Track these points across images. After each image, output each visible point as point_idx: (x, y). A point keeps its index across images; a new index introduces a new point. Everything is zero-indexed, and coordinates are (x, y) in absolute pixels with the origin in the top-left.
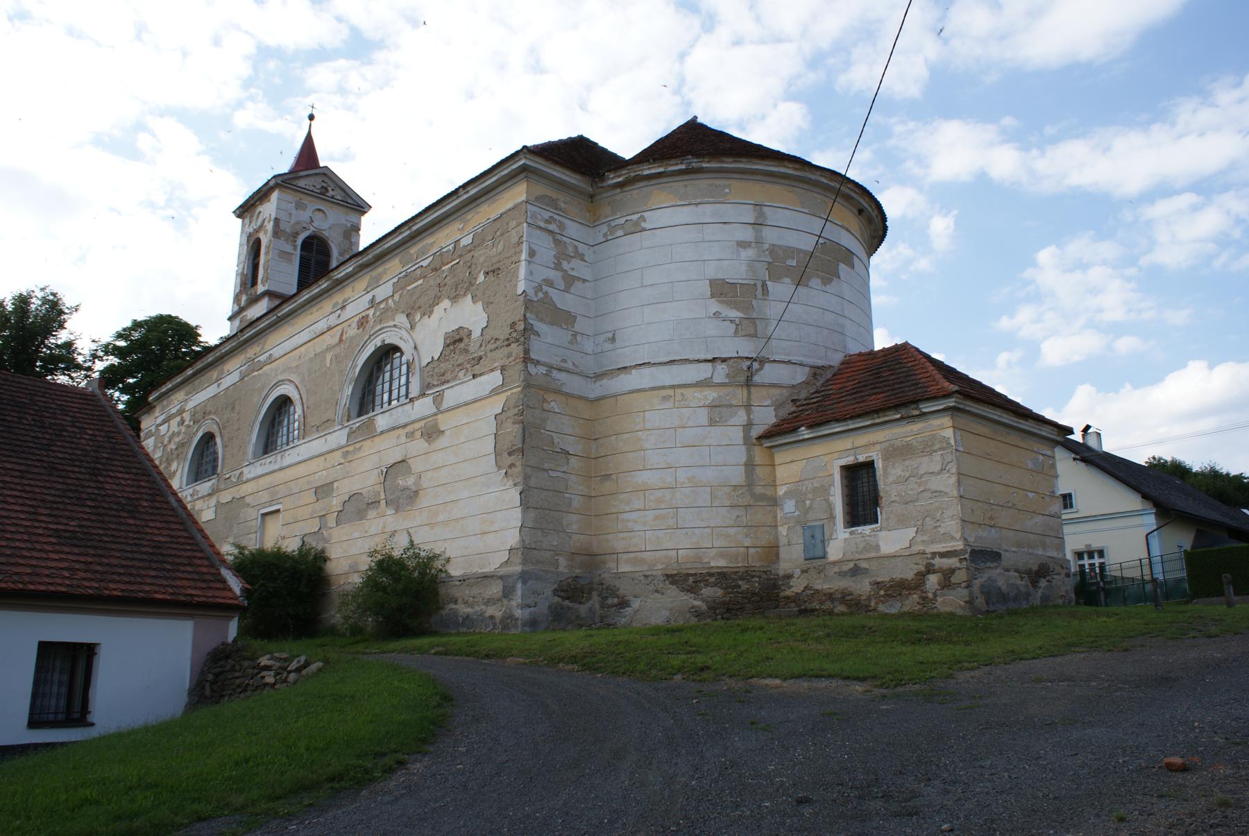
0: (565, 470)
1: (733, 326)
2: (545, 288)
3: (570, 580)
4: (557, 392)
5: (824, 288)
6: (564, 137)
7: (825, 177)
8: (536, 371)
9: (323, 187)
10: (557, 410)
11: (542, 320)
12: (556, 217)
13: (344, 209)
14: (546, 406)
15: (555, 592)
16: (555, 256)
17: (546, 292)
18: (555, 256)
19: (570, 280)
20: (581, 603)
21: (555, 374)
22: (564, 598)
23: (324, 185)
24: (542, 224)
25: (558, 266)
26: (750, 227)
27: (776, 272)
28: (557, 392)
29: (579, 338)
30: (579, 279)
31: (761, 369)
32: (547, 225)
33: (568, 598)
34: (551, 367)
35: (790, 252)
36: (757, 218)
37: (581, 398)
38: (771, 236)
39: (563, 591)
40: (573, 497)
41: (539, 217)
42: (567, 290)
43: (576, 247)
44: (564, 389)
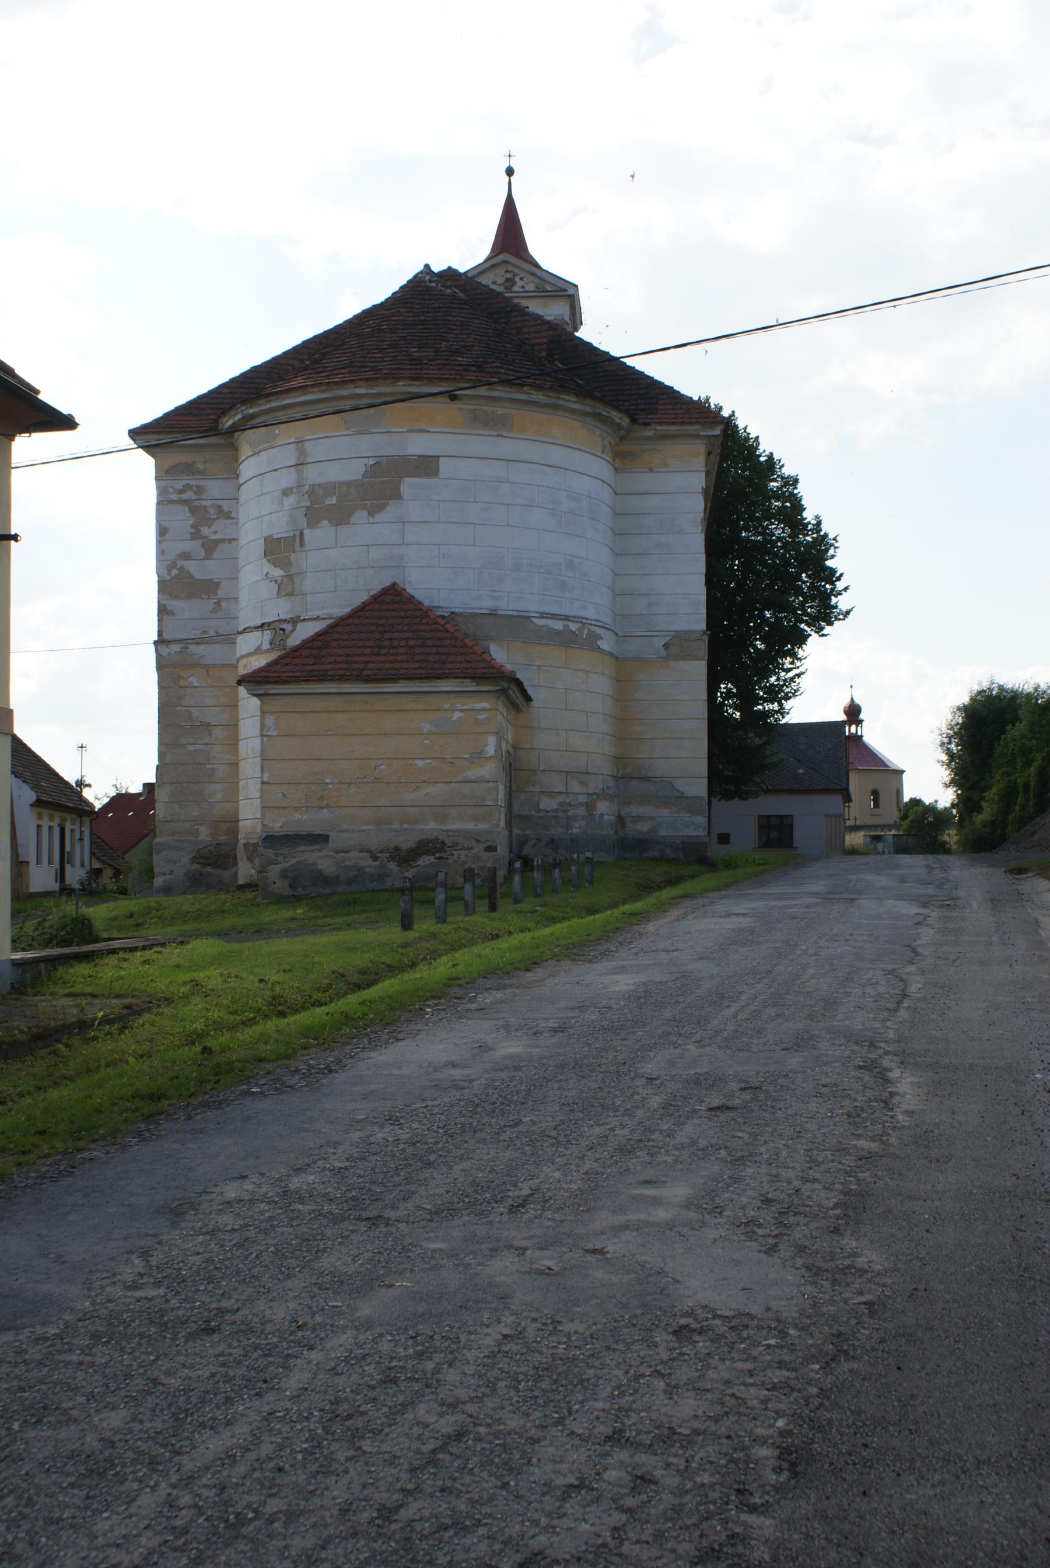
0: (206, 741)
1: (276, 586)
2: (180, 563)
3: (211, 848)
4: (196, 665)
5: (371, 520)
6: (396, 288)
7: (362, 387)
8: (168, 651)
9: (507, 280)
10: (196, 684)
11: (177, 597)
12: (191, 483)
13: (542, 301)
14: (182, 683)
15: (194, 860)
16: (192, 526)
17: (182, 567)
18: (192, 526)
19: (210, 547)
20: (225, 868)
21: (193, 649)
22: (204, 865)
23: (509, 276)
24: (174, 497)
25: (196, 535)
26: (293, 469)
27: (314, 515)
28: (196, 665)
29: (224, 604)
30: (223, 541)
31: (294, 630)
32: (181, 496)
33: (209, 865)
34: (184, 642)
35: (331, 488)
36: (298, 458)
37: (224, 666)
38: (314, 475)
39: (202, 858)
40: (216, 767)
41: (171, 490)
42: (208, 557)
43: (220, 507)
44: (203, 662)
